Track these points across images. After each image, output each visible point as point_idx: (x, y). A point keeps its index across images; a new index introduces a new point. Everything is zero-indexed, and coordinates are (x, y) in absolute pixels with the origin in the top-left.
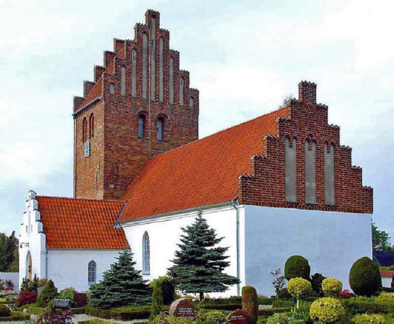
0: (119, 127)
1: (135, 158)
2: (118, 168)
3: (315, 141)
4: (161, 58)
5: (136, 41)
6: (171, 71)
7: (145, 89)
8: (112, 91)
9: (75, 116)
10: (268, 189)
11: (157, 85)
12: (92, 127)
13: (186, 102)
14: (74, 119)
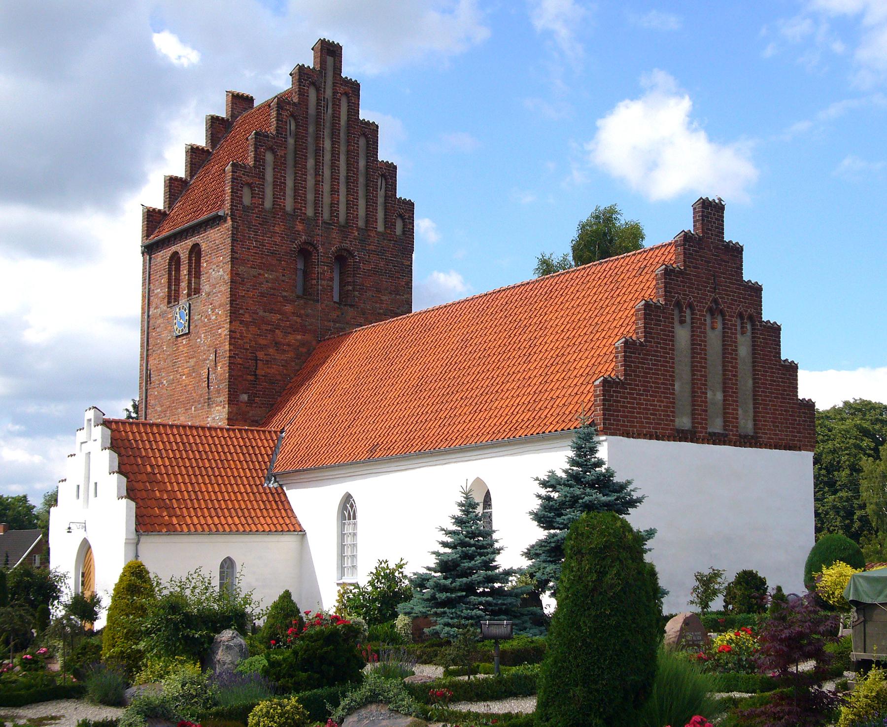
0: (260, 274)
1: (291, 338)
2: (256, 360)
3: (722, 313)
4: (342, 135)
5: (296, 100)
6: (362, 163)
7: (310, 197)
8: (247, 200)
9: (149, 250)
10: (646, 404)
11: (334, 191)
12: (196, 272)
13: (389, 224)
14: (143, 253)
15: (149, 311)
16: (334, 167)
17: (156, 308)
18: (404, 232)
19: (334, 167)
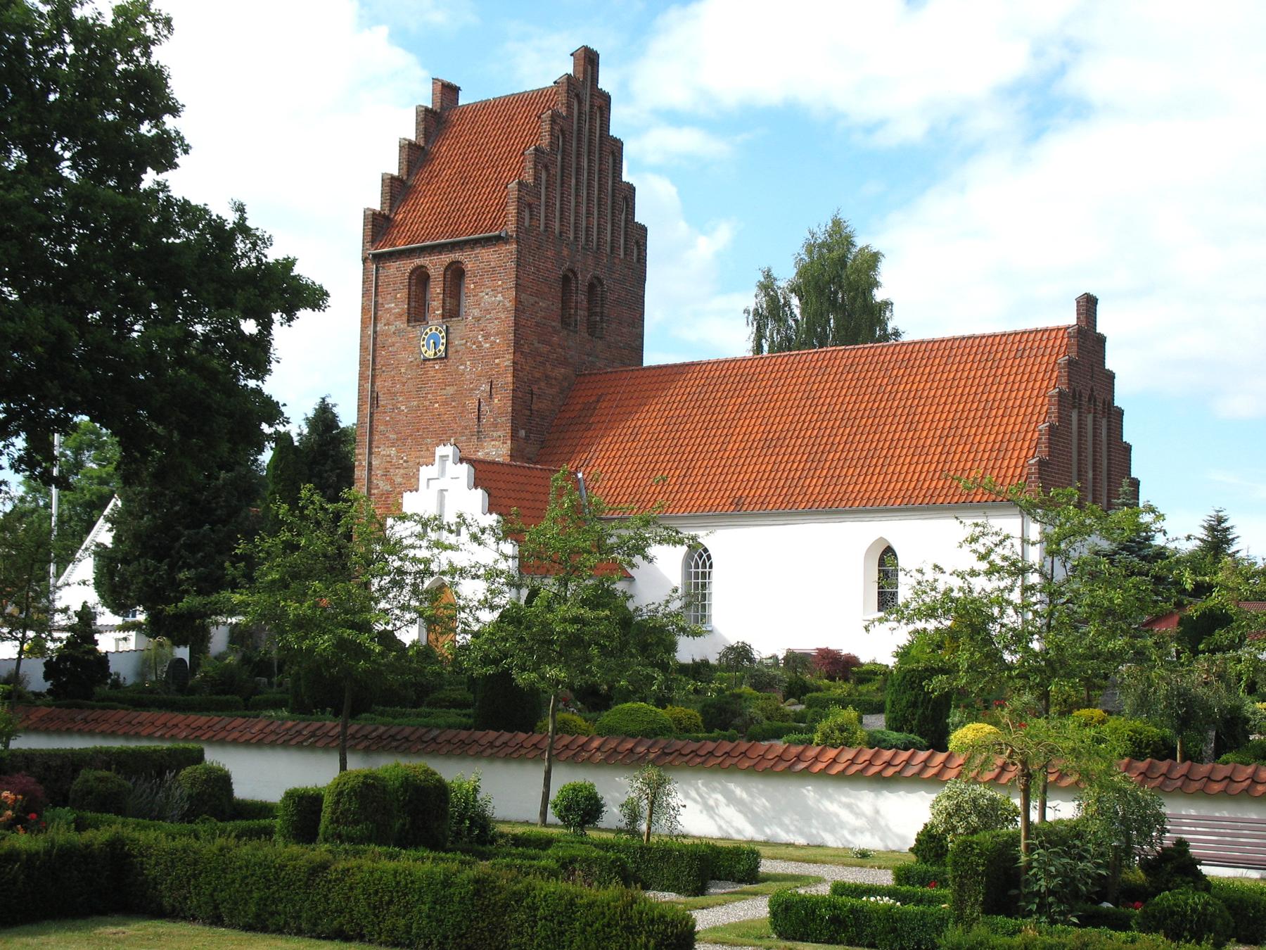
15: (375, 326)
16: (589, 186)
17: (387, 324)
18: (638, 260)
19: (589, 186)
